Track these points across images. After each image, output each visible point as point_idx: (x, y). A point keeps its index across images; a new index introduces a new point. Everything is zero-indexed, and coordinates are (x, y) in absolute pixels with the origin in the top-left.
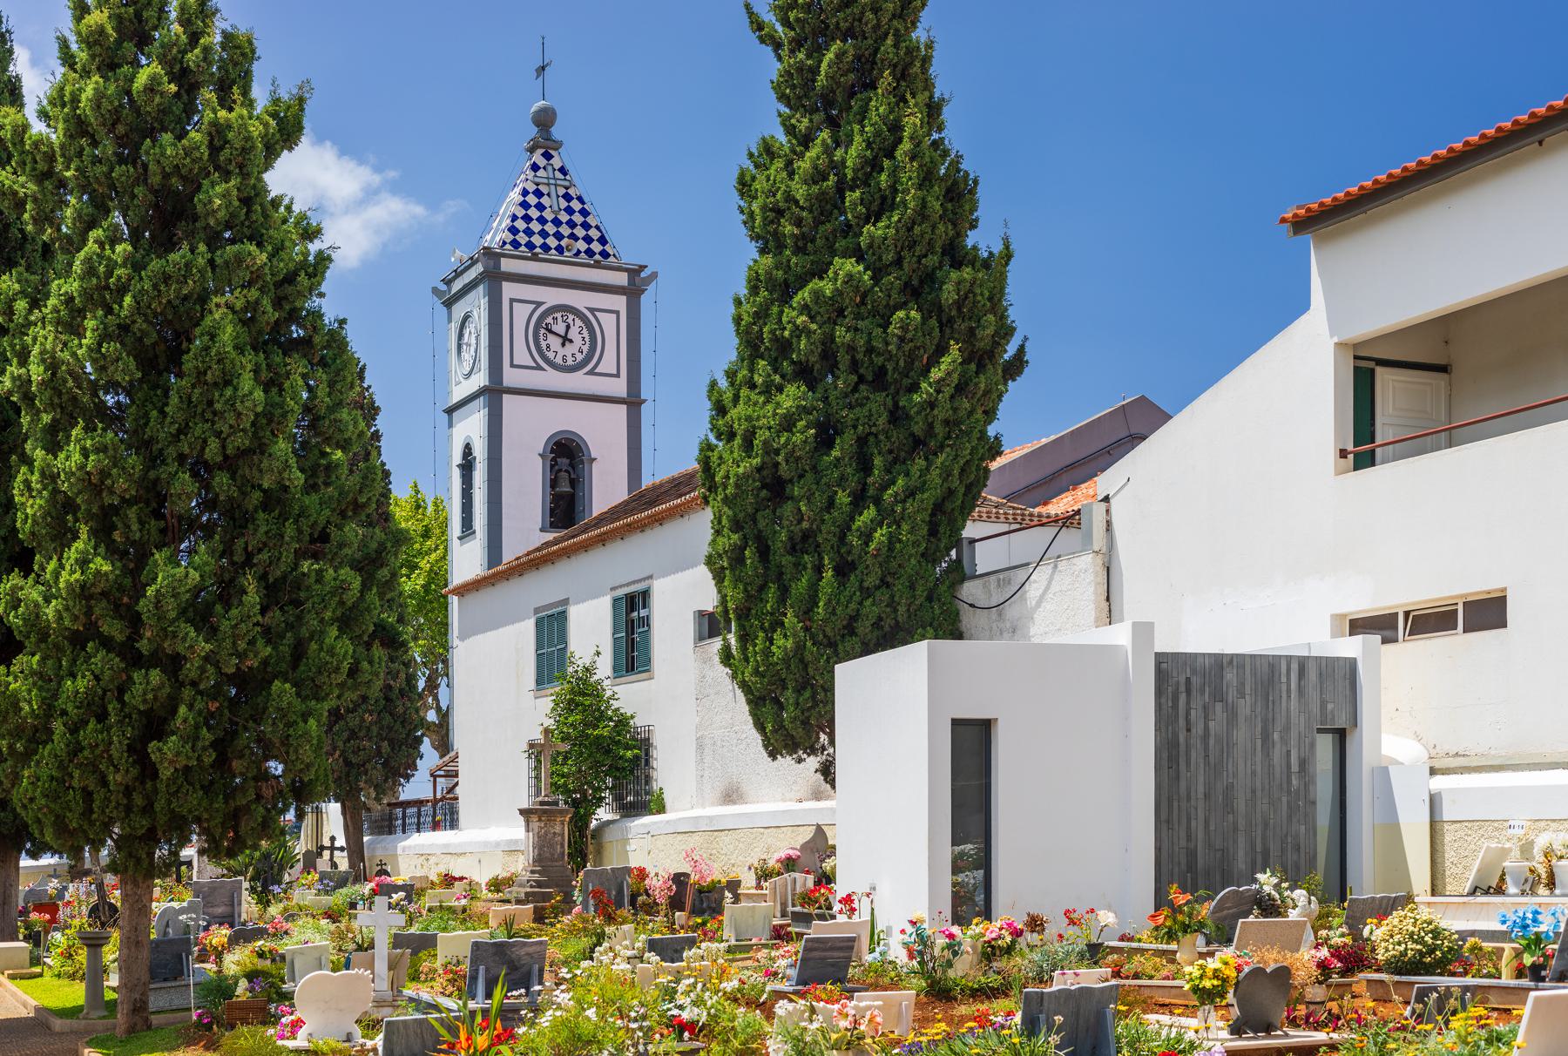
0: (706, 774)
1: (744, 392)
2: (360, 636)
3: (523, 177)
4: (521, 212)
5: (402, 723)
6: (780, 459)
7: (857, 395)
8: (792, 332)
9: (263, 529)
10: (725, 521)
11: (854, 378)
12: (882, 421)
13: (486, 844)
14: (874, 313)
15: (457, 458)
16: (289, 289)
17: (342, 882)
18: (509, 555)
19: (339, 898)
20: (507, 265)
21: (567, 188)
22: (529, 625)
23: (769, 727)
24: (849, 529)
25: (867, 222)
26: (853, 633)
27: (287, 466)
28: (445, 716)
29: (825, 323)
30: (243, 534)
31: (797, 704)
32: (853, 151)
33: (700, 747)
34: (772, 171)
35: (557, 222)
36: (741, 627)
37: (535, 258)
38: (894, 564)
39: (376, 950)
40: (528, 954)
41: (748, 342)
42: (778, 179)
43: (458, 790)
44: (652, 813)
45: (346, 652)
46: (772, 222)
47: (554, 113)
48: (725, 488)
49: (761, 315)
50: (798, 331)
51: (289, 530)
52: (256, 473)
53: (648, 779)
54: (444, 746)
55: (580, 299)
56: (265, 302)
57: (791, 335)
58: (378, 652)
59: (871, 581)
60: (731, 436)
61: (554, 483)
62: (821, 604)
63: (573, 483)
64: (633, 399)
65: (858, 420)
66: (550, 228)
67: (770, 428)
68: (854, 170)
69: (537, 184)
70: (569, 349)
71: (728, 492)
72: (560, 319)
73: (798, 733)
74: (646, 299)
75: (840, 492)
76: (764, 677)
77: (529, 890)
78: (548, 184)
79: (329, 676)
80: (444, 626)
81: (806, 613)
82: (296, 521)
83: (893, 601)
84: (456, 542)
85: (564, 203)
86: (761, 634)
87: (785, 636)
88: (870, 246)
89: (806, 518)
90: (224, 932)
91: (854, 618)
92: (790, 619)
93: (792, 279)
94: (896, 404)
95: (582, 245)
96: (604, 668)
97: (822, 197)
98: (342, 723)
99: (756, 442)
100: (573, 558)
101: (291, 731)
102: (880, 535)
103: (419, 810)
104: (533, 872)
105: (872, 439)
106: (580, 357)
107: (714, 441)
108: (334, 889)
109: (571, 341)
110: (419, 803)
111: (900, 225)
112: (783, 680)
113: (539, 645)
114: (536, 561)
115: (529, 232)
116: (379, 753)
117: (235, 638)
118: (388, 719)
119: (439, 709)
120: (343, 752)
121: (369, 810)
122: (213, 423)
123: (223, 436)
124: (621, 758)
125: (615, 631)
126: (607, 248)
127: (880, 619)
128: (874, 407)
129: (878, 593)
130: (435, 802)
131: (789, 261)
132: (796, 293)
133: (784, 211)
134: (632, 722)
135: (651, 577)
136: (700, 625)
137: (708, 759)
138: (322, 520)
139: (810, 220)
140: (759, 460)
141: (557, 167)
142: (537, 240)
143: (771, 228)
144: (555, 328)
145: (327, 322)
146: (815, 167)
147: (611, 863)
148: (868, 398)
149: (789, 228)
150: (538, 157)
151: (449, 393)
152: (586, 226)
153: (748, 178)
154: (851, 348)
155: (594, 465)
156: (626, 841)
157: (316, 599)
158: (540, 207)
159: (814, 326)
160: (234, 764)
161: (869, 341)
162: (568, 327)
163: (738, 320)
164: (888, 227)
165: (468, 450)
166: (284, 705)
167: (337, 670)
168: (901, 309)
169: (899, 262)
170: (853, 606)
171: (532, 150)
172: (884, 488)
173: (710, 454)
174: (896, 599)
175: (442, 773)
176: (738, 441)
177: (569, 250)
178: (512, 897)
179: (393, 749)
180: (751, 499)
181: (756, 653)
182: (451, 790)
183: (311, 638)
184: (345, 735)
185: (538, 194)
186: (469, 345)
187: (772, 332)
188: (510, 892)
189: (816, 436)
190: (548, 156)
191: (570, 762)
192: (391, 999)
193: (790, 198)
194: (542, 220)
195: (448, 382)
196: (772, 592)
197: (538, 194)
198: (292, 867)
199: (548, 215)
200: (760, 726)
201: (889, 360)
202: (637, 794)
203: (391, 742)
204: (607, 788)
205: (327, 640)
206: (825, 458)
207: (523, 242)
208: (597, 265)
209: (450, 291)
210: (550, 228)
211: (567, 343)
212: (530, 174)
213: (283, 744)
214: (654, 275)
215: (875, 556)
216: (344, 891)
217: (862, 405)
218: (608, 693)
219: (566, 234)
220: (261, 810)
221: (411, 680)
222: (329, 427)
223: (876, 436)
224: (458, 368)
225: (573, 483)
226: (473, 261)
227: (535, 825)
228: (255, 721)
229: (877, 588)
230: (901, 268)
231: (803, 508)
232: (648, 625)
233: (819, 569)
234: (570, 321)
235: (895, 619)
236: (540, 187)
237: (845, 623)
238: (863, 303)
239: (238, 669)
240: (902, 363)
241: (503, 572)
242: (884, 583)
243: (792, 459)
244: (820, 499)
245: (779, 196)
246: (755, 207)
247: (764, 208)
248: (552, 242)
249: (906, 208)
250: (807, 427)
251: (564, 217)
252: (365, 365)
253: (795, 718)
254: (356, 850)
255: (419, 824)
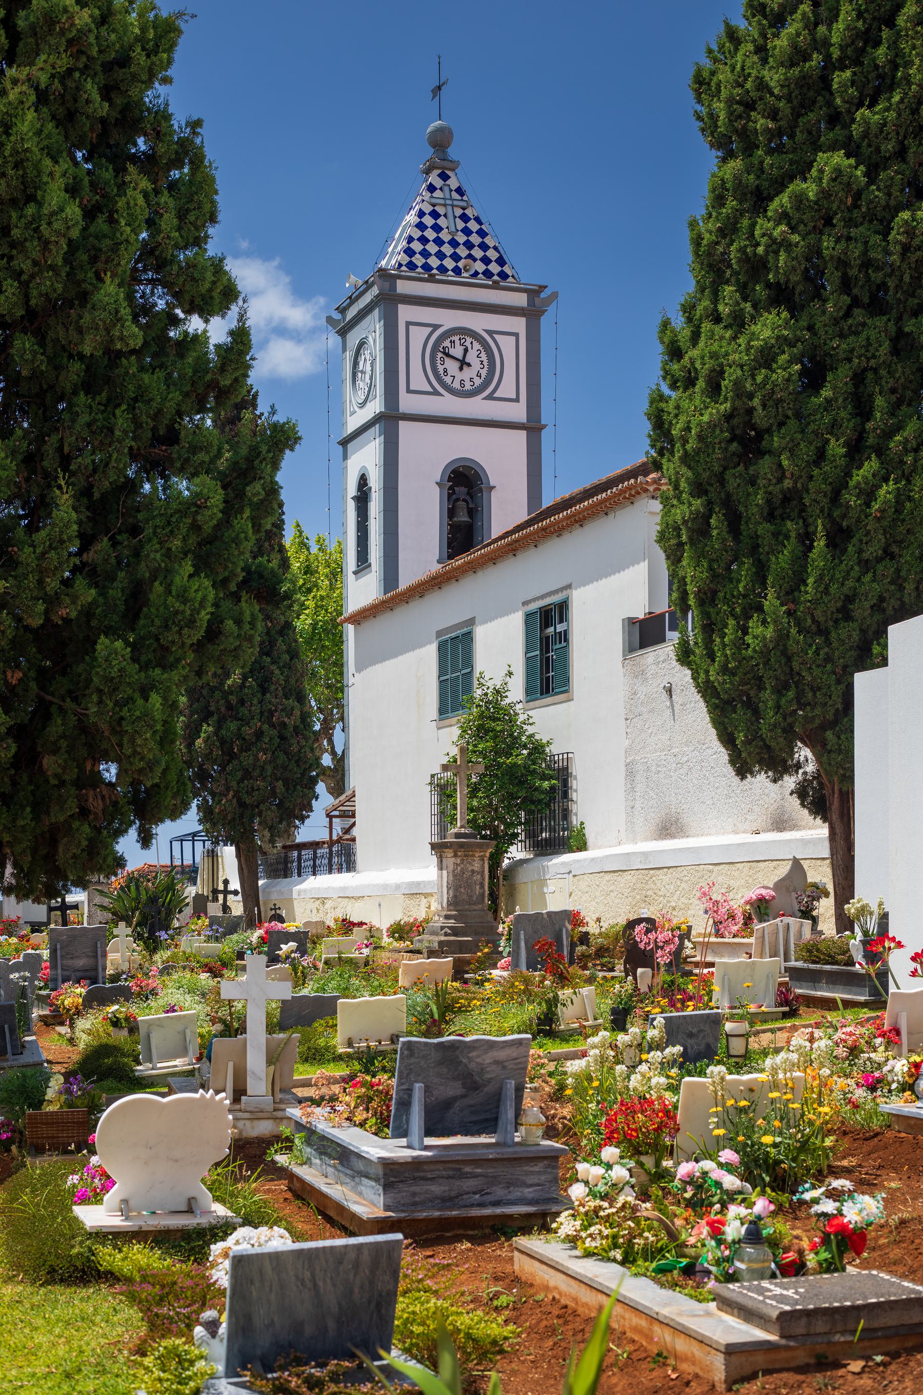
0: (638, 805)
1: (706, 326)
2: (225, 582)
3: (419, 199)
4: (417, 234)
5: (297, 762)
6: (756, 402)
7: (850, 321)
8: (768, 246)
9: (84, 418)
10: (683, 485)
11: (846, 299)
12: (884, 349)
13: (386, 886)
14: (871, 217)
15: (352, 490)
16: (120, 73)
17: (232, 927)
18: (405, 582)
19: (226, 947)
20: (403, 287)
21: (464, 209)
22: (430, 652)
23: (741, 737)
24: (846, 486)
25: (860, 105)
26: (848, 617)
27: (117, 319)
28: (341, 761)
29: (809, 233)
30: (57, 429)
31: (778, 707)
32: (840, 26)
33: (630, 773)
34: (739, 57)
35: (454, 243)
36: (705, 615)
37: (432, 279)
38: (902, 529)
39: (248, 1036)
40: (497, 1062)
41: (710, 266)
42: (748, 64)
43: (355, 832)
44: (571, 850)
45: (204, 598)
46: (740, 117)
47: (451, 133)
48: (685, 441)
49: (728, 231)
50: (776, 245)
51: (122, 420)
52: (73, 335)
53: (566, 814)
54: (339, 783)
55: (479, 322)
56: (89, 86)
57: (767, 252)
58: (249, 607)
59: (873, 550)
60: (690, 382)
61: (451, 513)
62: (810, 581)
63: (471, 512)
64: (533, 425)
65: (852, 351)
66: (447, 250)
67: (742, 366)
68: (841, 48)
69: (434, 205)
70: (467, 373)
71: (688, 447)
72: (457, 342)
73: (777, 742)
74: (546, 321)
75: (833, 441)
76: (734, 674)
77: (443, 938)
78: (445, 205)
79: (179, 632)
80: (339, 665)
81: (790, 593)
82: (132, 408)
83: (899, 577)
84: (351, 577)
85: (461, 225)
86: (731, 622)
87: (764, 622)
88: (865, 135)
89: (788, 474)
90: (78, 991)
91: (849, 599)
92: (770, 601)
93: (766, 184)
94: (900, 331)
95: (480, 267)
96: (516, 691)
97: (803, 82)
98: (235, 762)
99: (724, 383)
100: (480, 574)
101: (125, 712)
102: (886, 491)
103: (315, 853)
104: (447, 917)
105: (870, 375)
106: (478, 382)
107: (666, 390)
108: (224, 935)
109: (469, 365)
110: (315, 845)
111: (902, 106)
112: (760, 678)
113: (442, 671)
114: (435, 583)
115: (425, 254)
116: (273, 793)
117: (42, 573)
118: (282, 757)
119: (333, 753)
120: (236, 793)
121: (265, 854)
122: (11, 258)
123: (24, 277)
124: (536, 789)
125: (528, 648)
126: (506, 269)
127: (882, 599)
128: (873, 334)
129: (880, 567)
130: (331, 843)
131: (762, 163)
132: (771, 199)
133: (754, 102)
134: (547, 750)
135: (569, 587)
136: (630, 634)
137: (640, 788)
138: (170, 407)
139: (788, 111)
140: (728, 405)
141: (453, 188)
142: (434, 262)
143: (738, 125)
144: (452, 352)
145: (176, 127)
146: (794, 46)
147: (526, 906)
148: (864, 324)
149: (762, 121)
150: (434, 178)
151: (344, 424)
152: (484, 247)
153: (705, 74)
154: (842, 263)
155: (493, 493)
156: (543, 882)
157: (158, 521)
158: (437, 228)
159: (796, 238)
160: (45, 761)
161: (865, 253)
162: (466, 350)
163: (697, 241)
164: (887, 109)
165: (363, 481)
166: (114, 673)
167: (191, 623)
168: (903, 209)
169: (901, 153)
170: (850, 583)
171: (428, 172)
172: (888, 434)
173: (663, 405)
174: (903, 573)
175: (336, 813)
176: (701, 384)
177: (467, 271)
178: (423, 946)
179: (287, 789)
180: (718, 454)
181: (724, 645)
182: (347, 831)
183: (154, 578)
184: (239, 774)
185: (435, 215)
186: (363, 372)
187: (742, 250)
188: (421, 941)
189: (802, 373)
190: (444, 177)
191: (480, 794)
192: (270, 1108)
193: (762, 85)
194: (439, 242)
195: (343, 412)
196: (744, 571)
197: (435, 215)
198: (180, 911)
199: (445, 236)
200: (727, 739)
201: (890, 276)
202: (552, 830)
203: (286, 782)
204: (520, 824)
205: (177, 579)
206: (814, 399)
207: (419, 264)
208: (496, 286)
209: (344, 319)
210: (447, 250)
211: (465, 367)
212: (427, 195)
213: (114, 731)
214: (555, 295)
215: (878, 519)
216: (235, 937)
217: (857, 333)
218: (522, 718)
219: (463, 255)
220: (86, 828)
221: (305, 718)
222: (178, 275)
223: (875, 370)
224: (352, 397)
225: (471, 512)
226: (368, 285)
227: (450, 861)
228: (75, 700)
229: (879, 560)
230: (904, 160)
231: (785, 463)
232: (566, 640)
233: (807, 540)
234: (468, 344)
235: (900, 599)
236: (437, 208)
237: (839, 604)
238: (856, 206)
239: (48, 619)
240: (907, 278)
241: (402, 594)
242: (888, 554)
243: (770, 403)
244: (806, 451)
245: (748, 85)
246: (719, 107)
247: (730, 101)
248: (449, 264)
249: (909, 84)
250: (790, 362)
251: (461, 238)
252: (257, 392)
253: (775, 726)
254: (251, 894)
255: (314, 866)
